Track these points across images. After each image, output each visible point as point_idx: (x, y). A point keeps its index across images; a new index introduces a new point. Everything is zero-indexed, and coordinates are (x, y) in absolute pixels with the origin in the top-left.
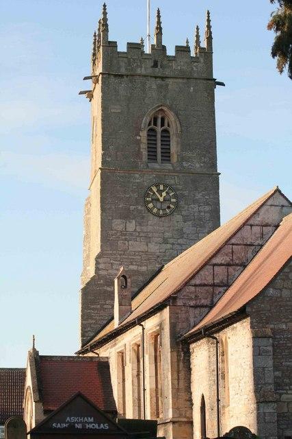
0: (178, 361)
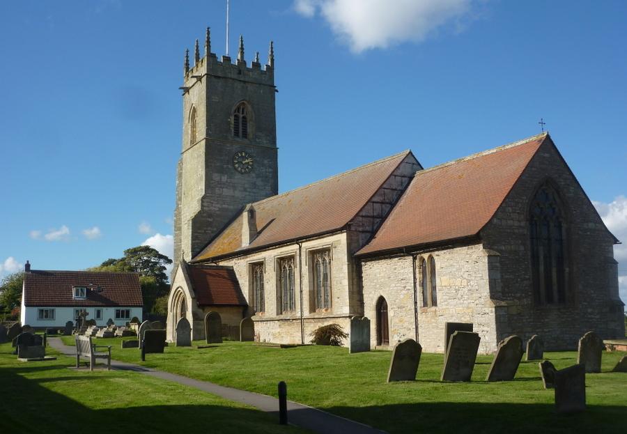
0: (352, 271)
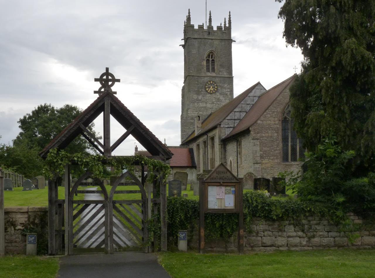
0: (222, 148)
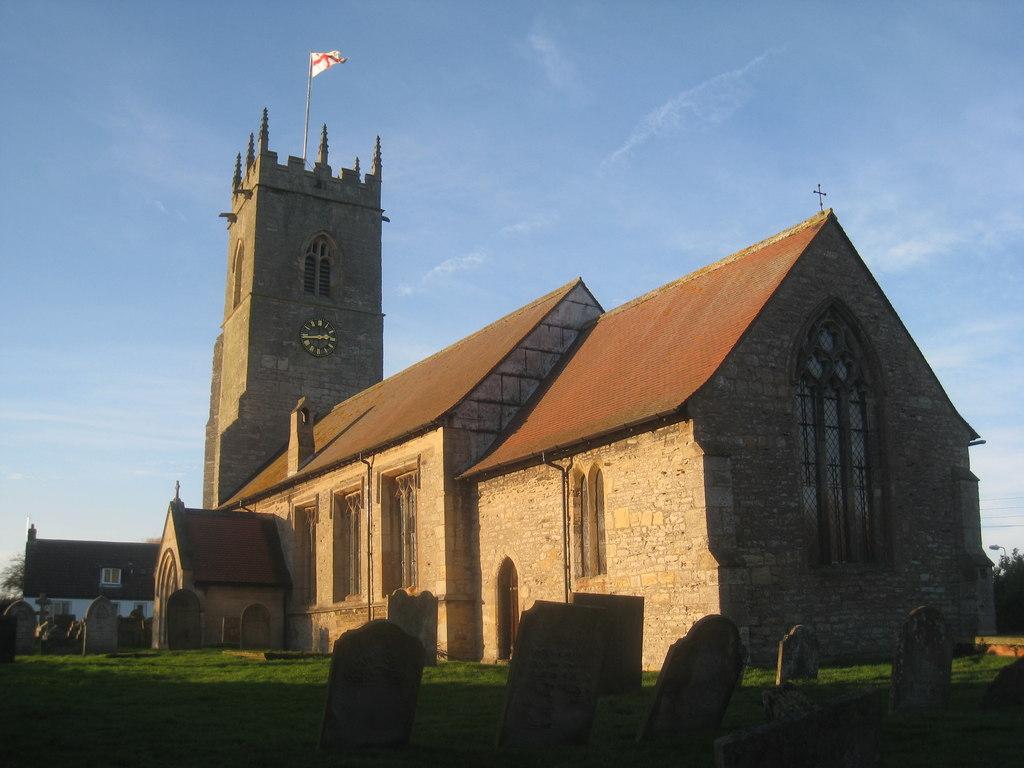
0: (455, 508)
